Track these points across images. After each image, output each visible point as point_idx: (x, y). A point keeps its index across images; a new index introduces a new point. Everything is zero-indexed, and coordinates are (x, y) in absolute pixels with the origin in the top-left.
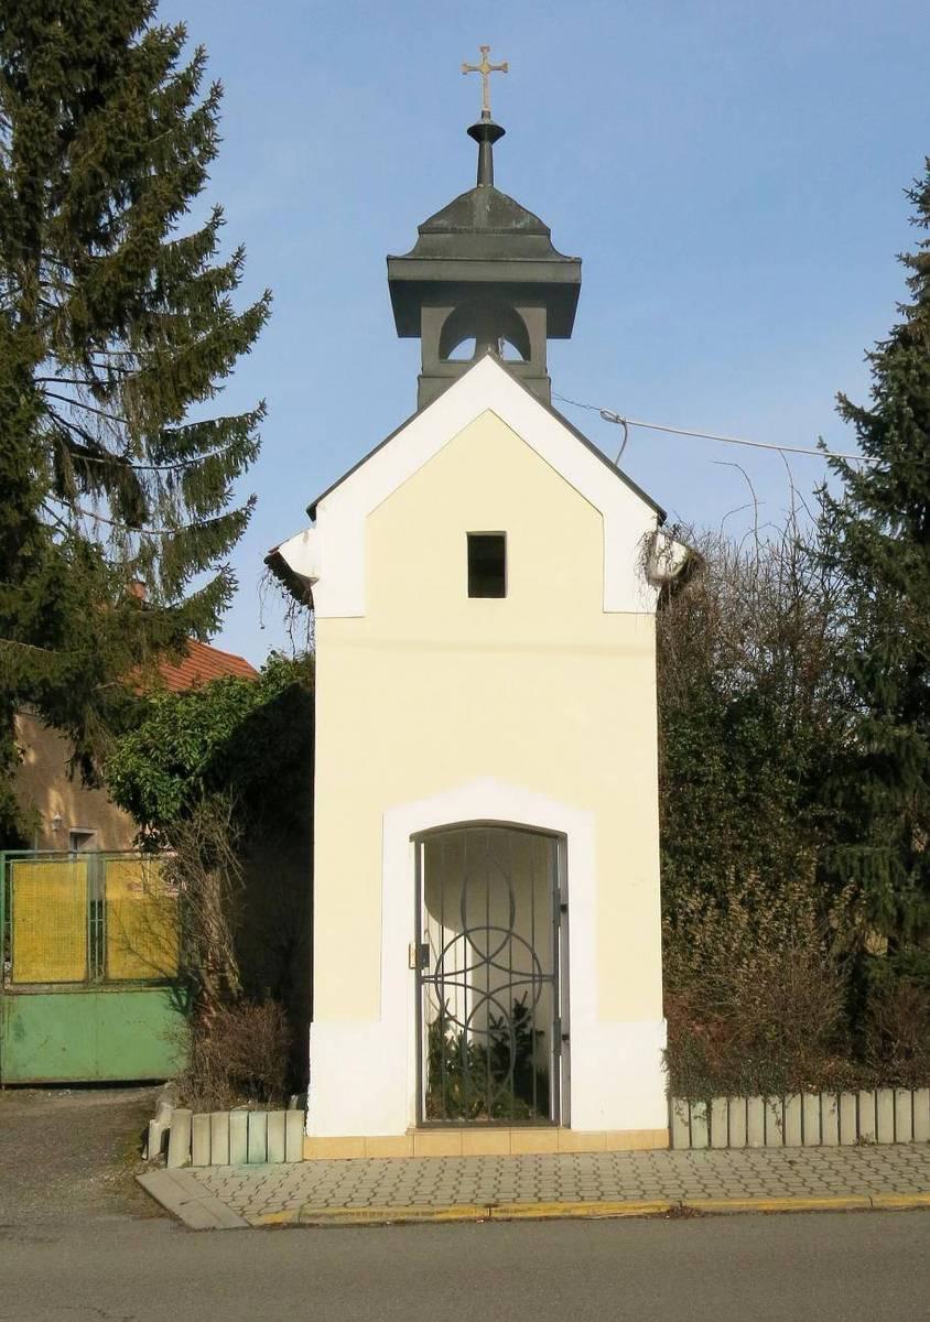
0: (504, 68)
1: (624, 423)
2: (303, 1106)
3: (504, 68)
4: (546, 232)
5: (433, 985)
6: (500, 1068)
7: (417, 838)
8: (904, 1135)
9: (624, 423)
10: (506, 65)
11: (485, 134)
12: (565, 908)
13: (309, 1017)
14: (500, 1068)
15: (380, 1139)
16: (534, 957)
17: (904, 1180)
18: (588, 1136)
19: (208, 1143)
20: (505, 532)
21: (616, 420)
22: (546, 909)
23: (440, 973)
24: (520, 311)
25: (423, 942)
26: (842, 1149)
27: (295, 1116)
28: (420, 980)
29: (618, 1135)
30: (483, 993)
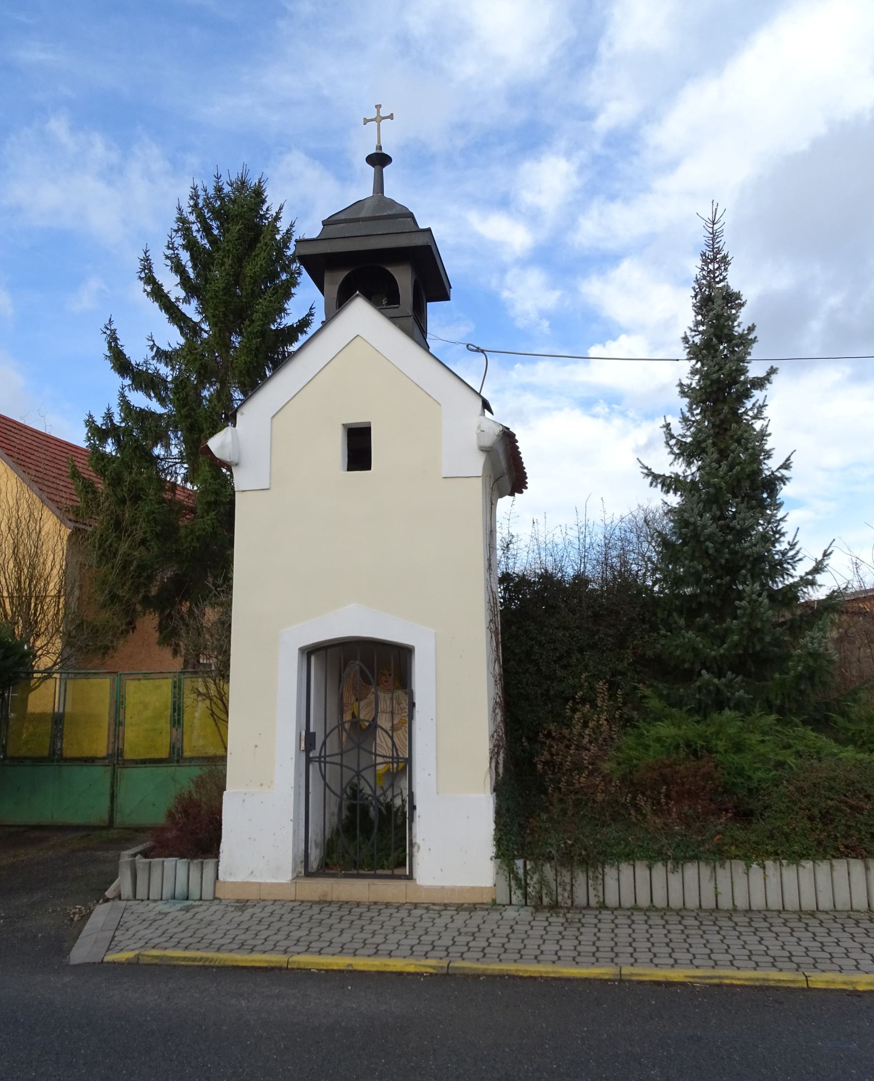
0: (391, 117)
1: (482, 351)
2: (217, 855)
3: (391, 117)
4: (411, 216)
5: (317, 764)
6: (364, 828)
7: (309, 652)
8: (741, 904)
9: (482, 351)
10: (376, 106)
11: (379, 160)
12: (414, 705)
13: (224, 788)
14: (364, 828)
15: (272, 885)
16: (394, 744)
17: (820, 939)
18: (430, 890)
19: (802, 889)
20: (370, 423)
21: (478, 350)
22: (405, 705)
23: (323, 754)
24: (389, 269)
25: (312, 730)
26: (768, 914)
27: (209, 864)
28: (308, 761)
29: (453, 890)
30: (354, 771)
